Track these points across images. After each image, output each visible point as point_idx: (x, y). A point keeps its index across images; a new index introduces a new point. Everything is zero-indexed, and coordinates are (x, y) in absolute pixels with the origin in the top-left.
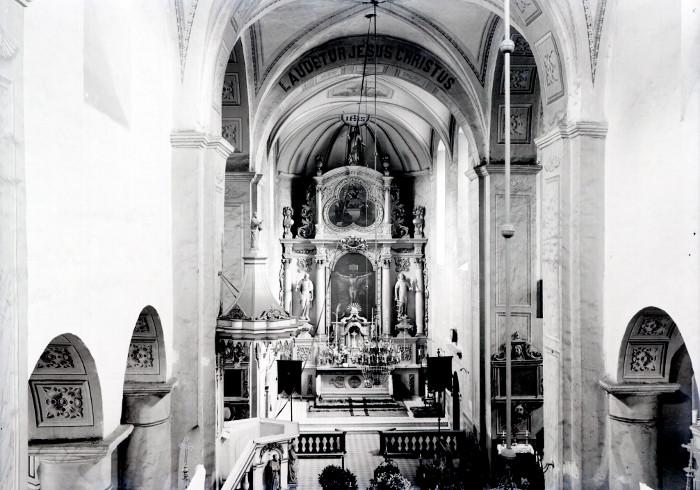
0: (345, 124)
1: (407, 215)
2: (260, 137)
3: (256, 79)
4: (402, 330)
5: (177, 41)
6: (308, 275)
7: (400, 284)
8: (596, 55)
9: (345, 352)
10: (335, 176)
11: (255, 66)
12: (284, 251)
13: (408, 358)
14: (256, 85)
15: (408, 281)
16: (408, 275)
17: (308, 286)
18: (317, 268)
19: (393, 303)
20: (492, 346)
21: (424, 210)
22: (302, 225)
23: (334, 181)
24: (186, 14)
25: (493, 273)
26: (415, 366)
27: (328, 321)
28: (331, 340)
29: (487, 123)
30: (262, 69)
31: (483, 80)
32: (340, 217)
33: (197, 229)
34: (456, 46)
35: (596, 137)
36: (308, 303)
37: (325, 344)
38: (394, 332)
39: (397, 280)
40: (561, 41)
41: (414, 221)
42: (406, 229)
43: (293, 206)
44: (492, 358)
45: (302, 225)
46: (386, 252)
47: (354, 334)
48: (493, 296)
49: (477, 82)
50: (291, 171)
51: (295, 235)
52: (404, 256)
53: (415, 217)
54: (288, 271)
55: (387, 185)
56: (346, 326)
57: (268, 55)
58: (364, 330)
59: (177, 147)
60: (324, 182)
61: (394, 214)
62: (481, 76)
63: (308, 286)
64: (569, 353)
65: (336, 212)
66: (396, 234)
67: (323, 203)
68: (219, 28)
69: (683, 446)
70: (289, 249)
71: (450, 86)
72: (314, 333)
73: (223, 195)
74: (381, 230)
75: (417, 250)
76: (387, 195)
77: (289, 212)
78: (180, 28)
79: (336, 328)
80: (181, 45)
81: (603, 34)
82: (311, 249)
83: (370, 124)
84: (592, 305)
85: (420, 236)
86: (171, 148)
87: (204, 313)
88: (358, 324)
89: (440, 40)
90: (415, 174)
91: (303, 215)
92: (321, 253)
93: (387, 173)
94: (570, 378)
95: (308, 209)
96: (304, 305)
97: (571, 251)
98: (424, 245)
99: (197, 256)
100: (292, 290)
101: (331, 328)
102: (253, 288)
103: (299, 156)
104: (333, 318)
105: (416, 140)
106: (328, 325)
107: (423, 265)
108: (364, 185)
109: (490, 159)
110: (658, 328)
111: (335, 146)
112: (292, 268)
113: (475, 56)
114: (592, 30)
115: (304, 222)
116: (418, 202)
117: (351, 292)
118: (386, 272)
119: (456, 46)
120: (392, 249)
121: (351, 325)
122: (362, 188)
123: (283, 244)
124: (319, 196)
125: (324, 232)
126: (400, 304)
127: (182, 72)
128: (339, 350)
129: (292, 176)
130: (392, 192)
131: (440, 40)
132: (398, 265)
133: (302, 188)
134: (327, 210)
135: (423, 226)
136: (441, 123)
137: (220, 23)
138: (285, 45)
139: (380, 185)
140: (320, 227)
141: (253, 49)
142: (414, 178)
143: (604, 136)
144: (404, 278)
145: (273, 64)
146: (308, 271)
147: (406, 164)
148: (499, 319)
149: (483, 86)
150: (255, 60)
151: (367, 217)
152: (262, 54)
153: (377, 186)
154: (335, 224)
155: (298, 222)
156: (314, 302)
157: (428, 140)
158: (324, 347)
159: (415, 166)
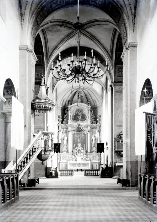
0: (77, 91)
1: (95, 119)
2: (47, 68)
3: (47, 58)
4: (94, 151)
5: (21, 20)
6: (66, 135)
7: (93, 138)
8: (134, 24)
9: (76, 157)
10: (74, 106)
11: (46, 54)
12: (59, 128)
13: (95, 159)
14: (47, 60)
15: (96, 137)
16: (95, 135)
17: (66, 138)
18: (68, 133)
19: (91, 143)
20: (115, 135)
21: (100, 116)
22: (64, 121)
23: (74, 108)
24: (23, 12)
25: (115, 114)
26: (97, 161)
27: (72, 149)
28: (72, 154)
29: (113, 72)
30: (49, 55)
31: (112, 58)
32: (75, 118)
33: (26, 72)
34: (104, 47)
35: (135, 47)
36: (66, 143)
37: (70, 155)
38: (91, 152)
39: (92, 137)
40: (126, 23)
41: (97, 119)
42: (95, 122)
43: (62, 115)
44: (115, 138)
45: (64, 121)
46: (89, 128)
47: (79, 152)
48: (115, 121)
49: (110, 59)
50: (61, 105)
51: (62, 123)
52: (94, 130)
53: (97, 118)
54: (60, 134)
55: (89, 108)
56: (77, 149)
57: (50, 50)
58: (82, 151)
59: (21, 50)
60: (71, 108)
61: (92, 118)
62: (111, 57)
63: (66, 138)
64: (128, 102)
65: (74, 117)
66: (92, 123)
67: (71, 114)
68: (32, 20)
69: (145, 88)
70: (60, 128)
71: (103, 62)
72: (67, 152)
73: (39, 94)
74: (88, 122)
75: (98, 128)
76: (89, 111)
77: (60, 117)
78: (21, 16)
79: (74, 151)
80: (22, 21)
81: (136, 17)
82: (67, 128)
83: (84, 90)
84: (133, 93)
85: (99, 124)
86: (19, 50)
87: (28, 97)
88: (80, 149)
89: (99, 45)
90: (98, 106)
91: (64, 118)
92: (70, 128)
93: (89, 105)
94: (128, 116)
95: (66, 116)
96: (64, 143)
97: (128, 80)
98: (100, 126)
99: (26, 79)
100: (61, 140)
101: (73, 151)
102: (42, 93)
103: (64, 101)
104: (73, 148)
105: (97, 93)
106: (72, 150)
107: (100, 132)
108: (83, 109)
109: (114, 81)
110: (149, 94)
111: (74, 98)
112: (61, 133)
113: (109, 51)
114: (133, 16)
115: (64, 120)
116: (98, 114)
117: (78, 141)
118: (89, 134)
119: (104, 47)
120: (91, 128)
121: (78, 149)
122: (82, 110)
123: (58, 126)
124: (69, 112)
125: (70, 122)
126: (93, 144)
127: (22, 29)
128: (75, 157)
129: (61, 106)
130: (91, 111)
131: (99, 45)
132: (92, 132)
133: (65, 110)
134: (71, 116)
135: (100, 121)
136: (103, 82)
137: (33, 19)
138: (55, 47)
139: (87, 108)
140: (69, 121)
141: (46, 48)
142: (97, 107)
143: (137, 47)
144: (94, 136)
145: (52, 53)
146: (66, 134)
147: (95, 103)
148: (116, 127)
149: (112, 60)
150: (46, 51)
151: (84, 118)
152: (49, 50)
153: (86, 108)
154: (74, 120)
155: (63, 120)
156: (67, 143)
157: (101, 93)
158: (70, 156)
159: (98, 103)
